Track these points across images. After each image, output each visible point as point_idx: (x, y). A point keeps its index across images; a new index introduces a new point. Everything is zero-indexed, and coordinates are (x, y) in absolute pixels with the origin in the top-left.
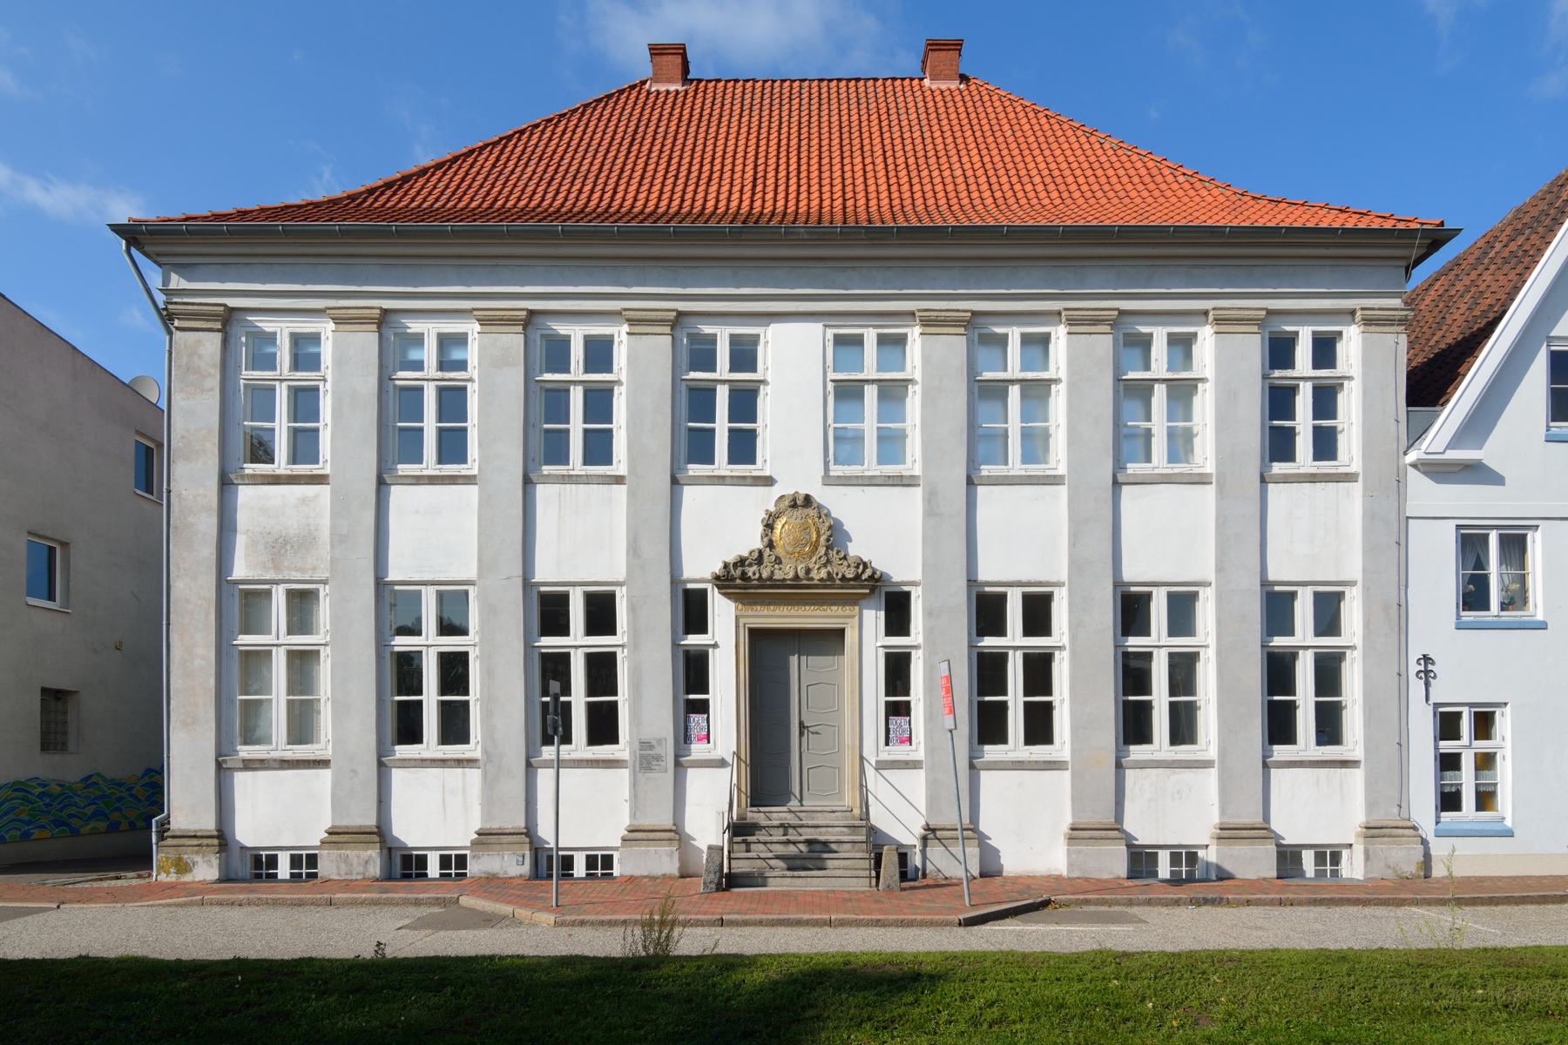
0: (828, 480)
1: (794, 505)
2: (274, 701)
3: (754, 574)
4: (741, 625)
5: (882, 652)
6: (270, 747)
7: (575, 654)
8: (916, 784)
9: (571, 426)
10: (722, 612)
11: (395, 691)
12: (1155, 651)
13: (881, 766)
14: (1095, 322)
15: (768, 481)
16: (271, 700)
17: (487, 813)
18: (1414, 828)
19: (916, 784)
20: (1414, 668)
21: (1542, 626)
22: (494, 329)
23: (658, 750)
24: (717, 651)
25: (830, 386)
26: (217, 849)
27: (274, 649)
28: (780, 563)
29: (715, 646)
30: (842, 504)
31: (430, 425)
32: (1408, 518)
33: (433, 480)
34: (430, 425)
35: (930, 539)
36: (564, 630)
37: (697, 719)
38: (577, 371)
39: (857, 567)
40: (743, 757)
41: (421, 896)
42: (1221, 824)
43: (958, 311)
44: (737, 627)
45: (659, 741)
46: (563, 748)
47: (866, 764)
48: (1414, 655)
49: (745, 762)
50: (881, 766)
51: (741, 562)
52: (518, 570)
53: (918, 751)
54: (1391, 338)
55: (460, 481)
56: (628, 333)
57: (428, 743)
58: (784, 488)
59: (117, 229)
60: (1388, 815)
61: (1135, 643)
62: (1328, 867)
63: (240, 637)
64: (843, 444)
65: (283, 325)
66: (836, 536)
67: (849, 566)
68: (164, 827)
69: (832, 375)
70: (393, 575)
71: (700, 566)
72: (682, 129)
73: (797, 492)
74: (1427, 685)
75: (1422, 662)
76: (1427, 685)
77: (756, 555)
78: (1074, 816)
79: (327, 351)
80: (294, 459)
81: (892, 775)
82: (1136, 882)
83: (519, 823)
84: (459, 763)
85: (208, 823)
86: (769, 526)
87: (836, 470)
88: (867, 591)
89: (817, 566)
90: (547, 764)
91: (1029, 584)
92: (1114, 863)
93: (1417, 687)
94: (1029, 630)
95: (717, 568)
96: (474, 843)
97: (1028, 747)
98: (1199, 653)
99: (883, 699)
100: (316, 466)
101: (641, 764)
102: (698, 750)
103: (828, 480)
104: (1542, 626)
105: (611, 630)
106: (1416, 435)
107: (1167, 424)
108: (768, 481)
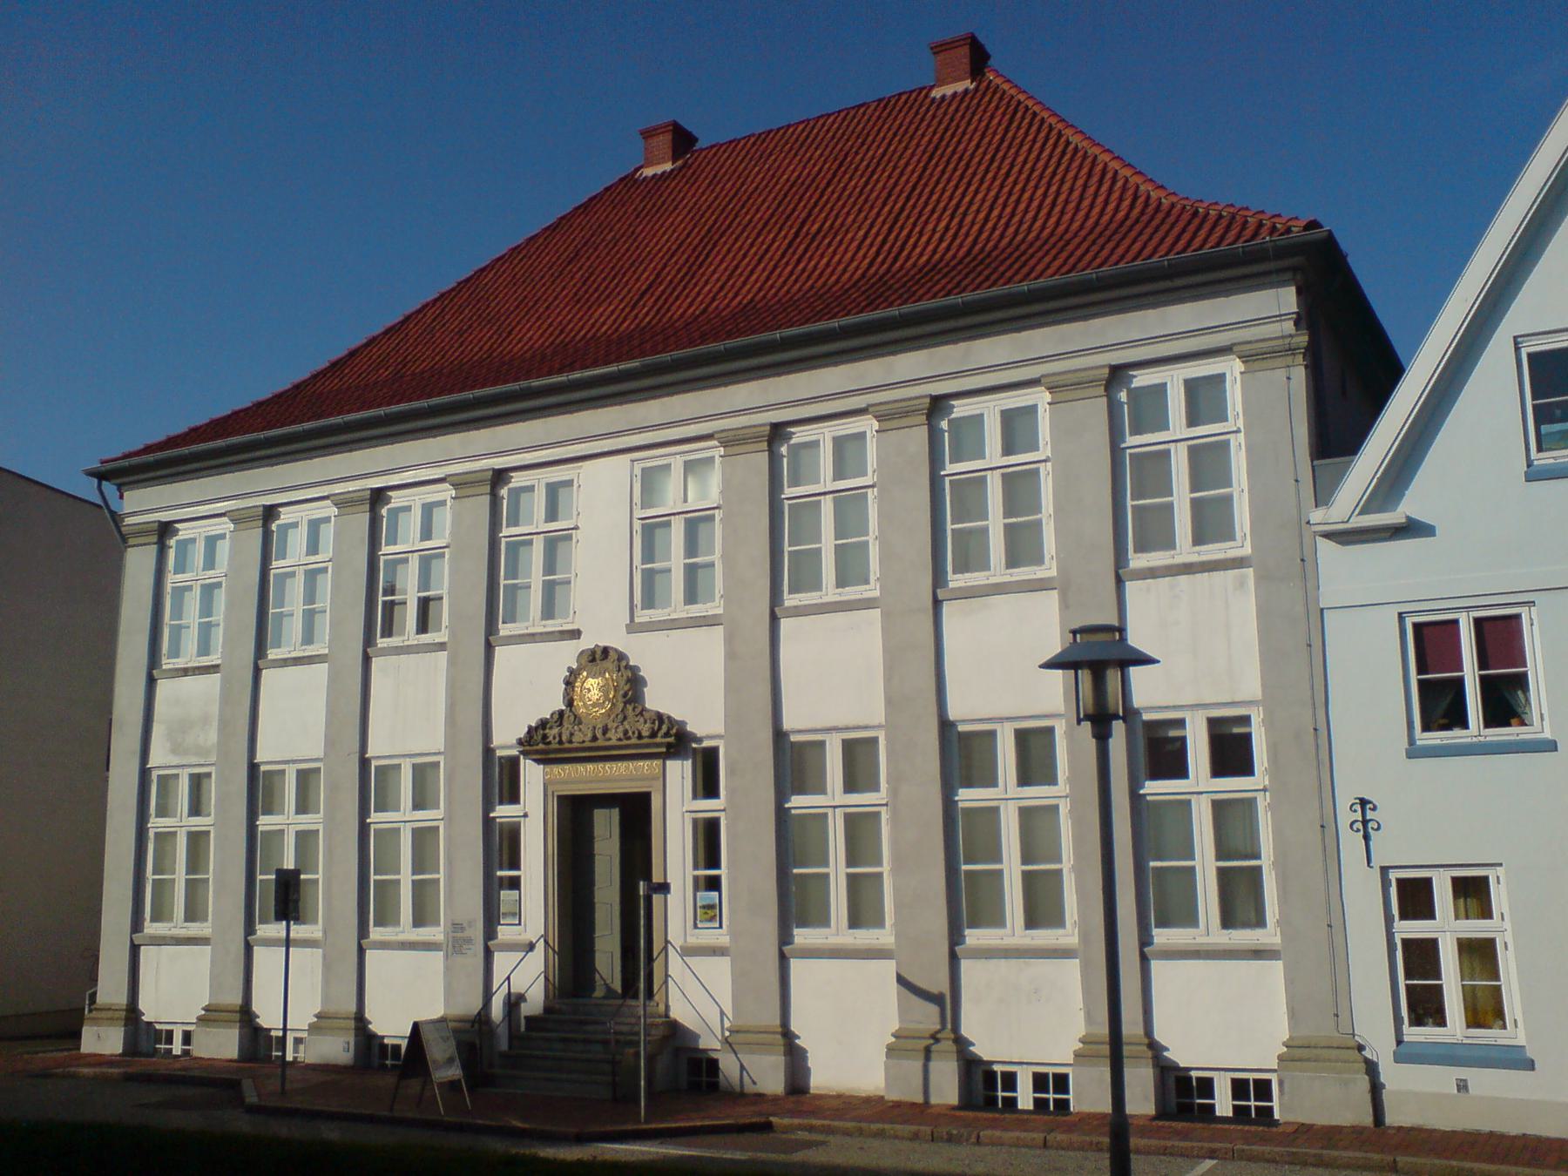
0: (633, 627)
1: (593, 660)
2: (832, 878)
3: (554, 738)
4: (550, 793)
5: (688, 817)
6: (172, 925)
7: (1006, 807)
8: (718, 973)
9: (1175, 499)
10: (532, 775)
11: (701, 862)
12: (1002, 805)
13: (688, 951)
14: (906, 414)
15: (575, 634)
16: (316, 881)
17: (326, 998)
18: (1361, 1048)
19: (718, 973)
20: (1346, 816)
21: (1551, 746)
22: (895, 423)
23: (467, 933)
24: (527, 819)
25: (637, 525)
26: (123, 1023)
27: (1194, 798)
28: (580, 723)
29: (525, 816)
30: (643, 652)
31: (1181, 497)
32: (1322, 610)
33: (1188, 569)
34: (1181, 497)
35: (732, 687)
36: (1179, 770)
37: (506, 895)
38: (826, 481)
39: (653, 723)
40: (551, 943)
41: (836, 1123)
42: (209, 1005)
43: (885, 403)
44: (545, 795)
45: (470, 924)
46: (293, 927)
47: (670, 947)
48: (1345, 800)
49: (554, 950)
50: (688, 951)
51: (543, 724)
52: (356, 746)
53: (1268, 936)
54: (1281, 374)
55: (317, 660)
56: (1049, 404)
57: (525, 925)
58: (587, 643)
59: (91, 473)
60: (1320, 1028)
61: (503, 812)
62: (704, 1079)
63: (1148, 783)
64: (650, 589)
65: (303, 514)
66: (632, 686)
67: (645, 722)
68: (93, 997)
69: (639, 513)
70: (788, 723)
71: (507, 734)
72: (1054, 160)
73: (597, 645)
74: (1366, 837)
75: (1358, 807)
76: (1366, 837)
77: (556, 717)
78: (901, 1020)
79: (1235, 395)
80: (1012, 561)
81: (698, 963)
82: (970, 1114)
83: (236, 999)
84: (1258, 954)
85: (122, 999)
86: (569, 683)
87: (643, 616)
88: (664, 750)
89: (615, 725)
90: (269, 942)
91: (847, 729)
92: (947, 1089)
93: (1351, 844)
94: (1026, 777)
95: (522, 732)
96: (200, 1019)
97: (851, 931)
98: (1256, 798)
99: (691, 873)
100: (867, 587)
101: (454, 947)
102: (505, 933)
103: (633, 627)
104: (1551, 746)
105: (1246, 768)
106: (1322, 497)
107: (407, 597)
108: (575, 634)
